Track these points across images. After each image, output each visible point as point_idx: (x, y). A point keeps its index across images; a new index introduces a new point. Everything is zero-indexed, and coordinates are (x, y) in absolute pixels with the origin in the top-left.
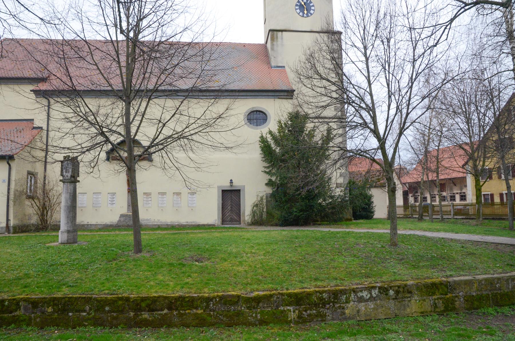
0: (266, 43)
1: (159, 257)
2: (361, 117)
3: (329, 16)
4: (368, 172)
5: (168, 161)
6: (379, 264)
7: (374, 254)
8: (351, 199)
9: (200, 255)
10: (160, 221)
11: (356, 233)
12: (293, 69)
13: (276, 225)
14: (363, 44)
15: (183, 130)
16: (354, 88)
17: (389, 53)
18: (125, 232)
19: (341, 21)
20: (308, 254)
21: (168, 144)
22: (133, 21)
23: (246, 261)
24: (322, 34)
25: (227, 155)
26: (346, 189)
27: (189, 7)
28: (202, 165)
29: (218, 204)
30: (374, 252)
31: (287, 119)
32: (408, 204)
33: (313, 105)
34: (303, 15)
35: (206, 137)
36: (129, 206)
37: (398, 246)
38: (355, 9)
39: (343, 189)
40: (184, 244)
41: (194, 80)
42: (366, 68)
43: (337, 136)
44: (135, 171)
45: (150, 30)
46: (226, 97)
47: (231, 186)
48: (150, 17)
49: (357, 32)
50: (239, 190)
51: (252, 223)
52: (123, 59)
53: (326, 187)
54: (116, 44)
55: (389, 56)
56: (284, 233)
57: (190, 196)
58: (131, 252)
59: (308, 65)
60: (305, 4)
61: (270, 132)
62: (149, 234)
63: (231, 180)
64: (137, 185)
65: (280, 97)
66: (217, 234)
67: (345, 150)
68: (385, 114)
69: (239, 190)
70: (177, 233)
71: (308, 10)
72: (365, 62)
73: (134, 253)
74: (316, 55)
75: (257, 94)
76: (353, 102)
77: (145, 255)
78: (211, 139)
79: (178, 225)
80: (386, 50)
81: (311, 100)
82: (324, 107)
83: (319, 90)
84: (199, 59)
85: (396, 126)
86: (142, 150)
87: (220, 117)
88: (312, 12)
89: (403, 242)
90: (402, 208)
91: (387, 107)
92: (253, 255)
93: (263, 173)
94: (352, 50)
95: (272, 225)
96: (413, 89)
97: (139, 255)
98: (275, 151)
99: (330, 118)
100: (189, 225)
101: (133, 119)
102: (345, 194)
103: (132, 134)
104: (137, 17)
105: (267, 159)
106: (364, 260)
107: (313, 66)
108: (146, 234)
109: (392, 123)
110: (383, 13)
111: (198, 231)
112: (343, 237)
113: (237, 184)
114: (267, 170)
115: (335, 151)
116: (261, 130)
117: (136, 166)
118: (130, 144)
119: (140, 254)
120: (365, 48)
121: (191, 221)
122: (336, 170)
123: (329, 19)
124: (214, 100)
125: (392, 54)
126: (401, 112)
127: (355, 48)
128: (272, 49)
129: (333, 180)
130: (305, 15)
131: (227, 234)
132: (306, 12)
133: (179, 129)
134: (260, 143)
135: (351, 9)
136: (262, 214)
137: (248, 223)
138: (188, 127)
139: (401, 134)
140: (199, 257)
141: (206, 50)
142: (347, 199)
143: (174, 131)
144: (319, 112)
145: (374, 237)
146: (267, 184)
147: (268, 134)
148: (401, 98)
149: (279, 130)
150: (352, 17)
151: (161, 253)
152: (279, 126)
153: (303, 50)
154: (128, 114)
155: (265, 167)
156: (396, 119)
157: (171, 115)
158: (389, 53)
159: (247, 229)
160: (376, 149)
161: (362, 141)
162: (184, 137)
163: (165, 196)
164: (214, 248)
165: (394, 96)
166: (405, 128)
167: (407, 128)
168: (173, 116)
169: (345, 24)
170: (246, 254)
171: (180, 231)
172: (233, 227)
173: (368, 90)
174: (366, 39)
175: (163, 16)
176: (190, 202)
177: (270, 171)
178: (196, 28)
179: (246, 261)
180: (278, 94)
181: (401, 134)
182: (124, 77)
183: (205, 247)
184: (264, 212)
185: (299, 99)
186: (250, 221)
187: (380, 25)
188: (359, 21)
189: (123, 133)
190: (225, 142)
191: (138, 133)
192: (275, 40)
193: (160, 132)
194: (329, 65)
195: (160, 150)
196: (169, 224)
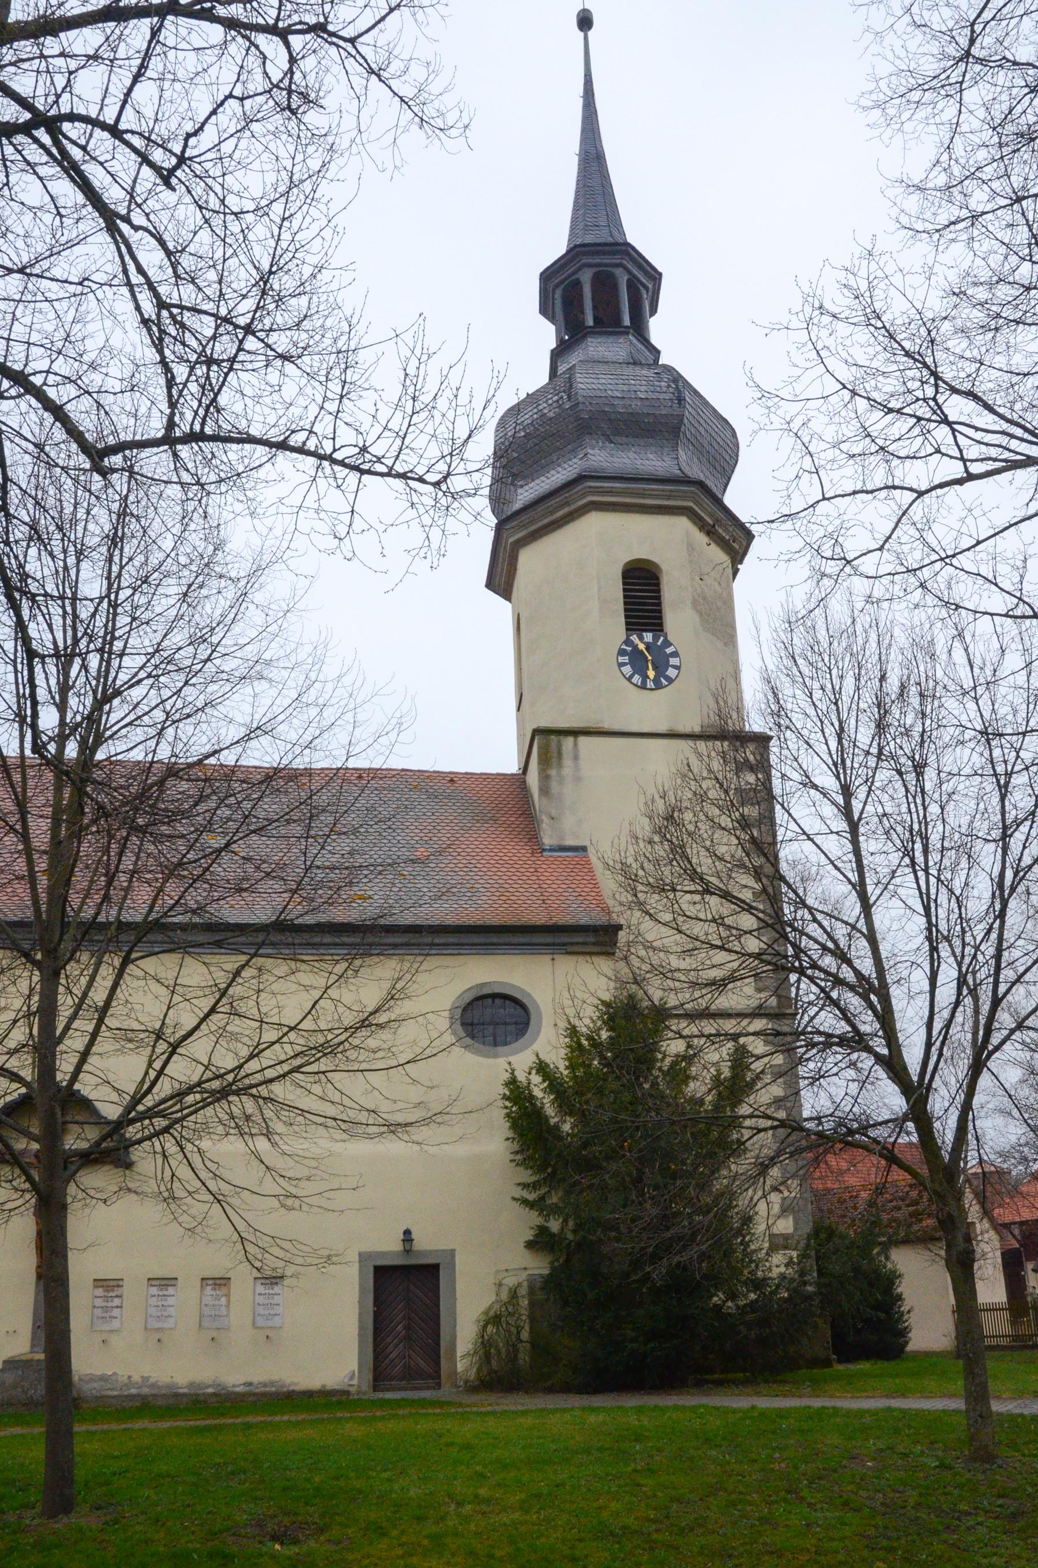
0: (525, 769)
1: (138, 1528)
2: (845, 1015)
3: (724, 692)
4: (880, 1190)
5: (183, 1172)
6: (935, 1533)
7: (912, 1496)
8: (823, 1290)
9: (288, 1514)
10: (152, 1380)
11: (849, 1413)
12: (611, 863)
13: (567, 1389)
14: (838, 777)
15: (240, 1067)
16: (815, 920)
17: (925, 809)
18: (18, 1430)
19: (763, 706)
20: (679, 1501)
21: (185, 1112)
22: (79, 705)
23: (456, 1534)
24: (701, 745)
25: (394, 1147)
26: (803, 1256)
27: (268, 663)
28: (302, 1184)
29: (360, 1314)
30: (913, 1488)
31: (599, 1023)
32: (1025, 1297)
33: (683, 978)
34: (644, 682)
35: (317, 1089)
36: (36, 1327)
37: (1000, 1462)
38: (806, 670)
39: (794, 1254)
40: (233, 1473)
41: (280, 900)
42: (851, 856)
43: (768, 1078)
44: (64, 1207)
45: (138, 734)
46: (387, 950)
47: (408, 1251)
48: (137, 693)
49: (816, 737)
50: (436, 1267)
51: (482, 1381)
52: (40, 830)
53: (735, 1252)
54: (17, 777)
55: (925, 817)
56: (592, 1419)
57: (260, 1289)
58: (30, 1513)
59: (661, 851)
60: (647, 649)
61: (542, 1068)
62: (106, 1432)
63: (407, 1232)
64: (72, 1257)
65: (570, 949)
66: (353, 1430)
67: (792, 1125)
68: (920, 1004)
69: (436, 1267)
70: (208, 1429)
71: (661, 667)
72: (848, 836)
73: (41, 1515)
74: (688, 816)
75: (495, 939)
76: (814, 966)
77: (83, 1522)
78: (337, 1097)
79: (214, 1394)
80: (914, 797)
81: (675, 962)
82: (720, 985)
83: (698, 929)
84: (297, 829)
85: (962, 1034)
86: (92, 1134)
87: (364, 1024)
88: (671, 672)
89: (1012, 1445)
90: (1006, 1315)
91: (927, 982)
92: (484, 1507)
93: (516, 1205)
94: (805, 799)
95: (551, 1390)
96: (1009, 921)
97: (61, 1524)
98: (557, 1127)
99: (741, 1015)
100: (255, 1394)
101: (67, 1028)
102: (802, 1273)
103: (59, 1076)
104: (95, 692)
105: (530, 1158)
106: (879, 1521)
107: (679, 851)
108: (94, 1433)
109: (947, 1033)
110: (897, 684)
111: (286, 1418)
112: (802, 1431)
113: (426, 1242)
114: (531, 1197)
115: (759, 1131)
116: (511, 1059)
117: (72, 1189)
118: (53, 1114)
119: (65, 1520)
120: (847, 791)
121: (261, 1380)
122: (764, 1196)
123: (725, 702)
124: (345, 965)
125: (934, 809)
126: (974, 993)
127: (812, 792)
128: (545, 791)
129: (760, 1227)
130: (650, 684)
131: (392, 1426)
132: (651, 674)
133: (228, 1062)
134: (507, 1104)
135: (795, 670)
136: (516, 1352)
137: (466, 1382)
138: (257, 1055)
139: (977, 1067)
140: (286, 1520)
141: (323, 799)
142: (810, 1289)
143: (207, 1068)
144: (703, 999)
145: (909, 1427)
146: (530, 1245)
147: (534, 1072)
148: (968, 950)
149: (569, 1059)
150: (798, 692)
151: (143, 1513)
152: (570, 1047)
153: (642, 800)
154: (47, 1010)
155: (525, 1186)
156: (959, 1018)
157: (202, 1015)
158: (925, 809)
159: (461, 1405)
160: (899, 1123)
161: (854, 1088)
162: (244, 1091)
163: (171, 1290)
164: (342, 1483)
165: (949, 941)
166: (990, 1048)
167: (997, 1048)
168: (207, 1016)
169: (778, 712)
170: (459, 1504)
171: (221, 1421)
172: (413, 1401)
173: (862, 924)
174: (848, 763)
175: (180, 690)
176: (260, 1310)
177: (542, 1198)
178: (289, 732)
179: (456, 1534)
180: (565, 938)
181: (977, 1067)
182: (43, 881)
183: (308, 1480)
184: (522, 1341)
185: (635, 962)
186: (472, 1374)
187: (889, 719)
188: (822, 706)
189: (27, 1074)
190: (384, 1106)
191: (82, 1075)
192: (554, 760)
193: (160, 1073)
194: (728, 846)
195: (157, 1134)
196: (181, 1391)
